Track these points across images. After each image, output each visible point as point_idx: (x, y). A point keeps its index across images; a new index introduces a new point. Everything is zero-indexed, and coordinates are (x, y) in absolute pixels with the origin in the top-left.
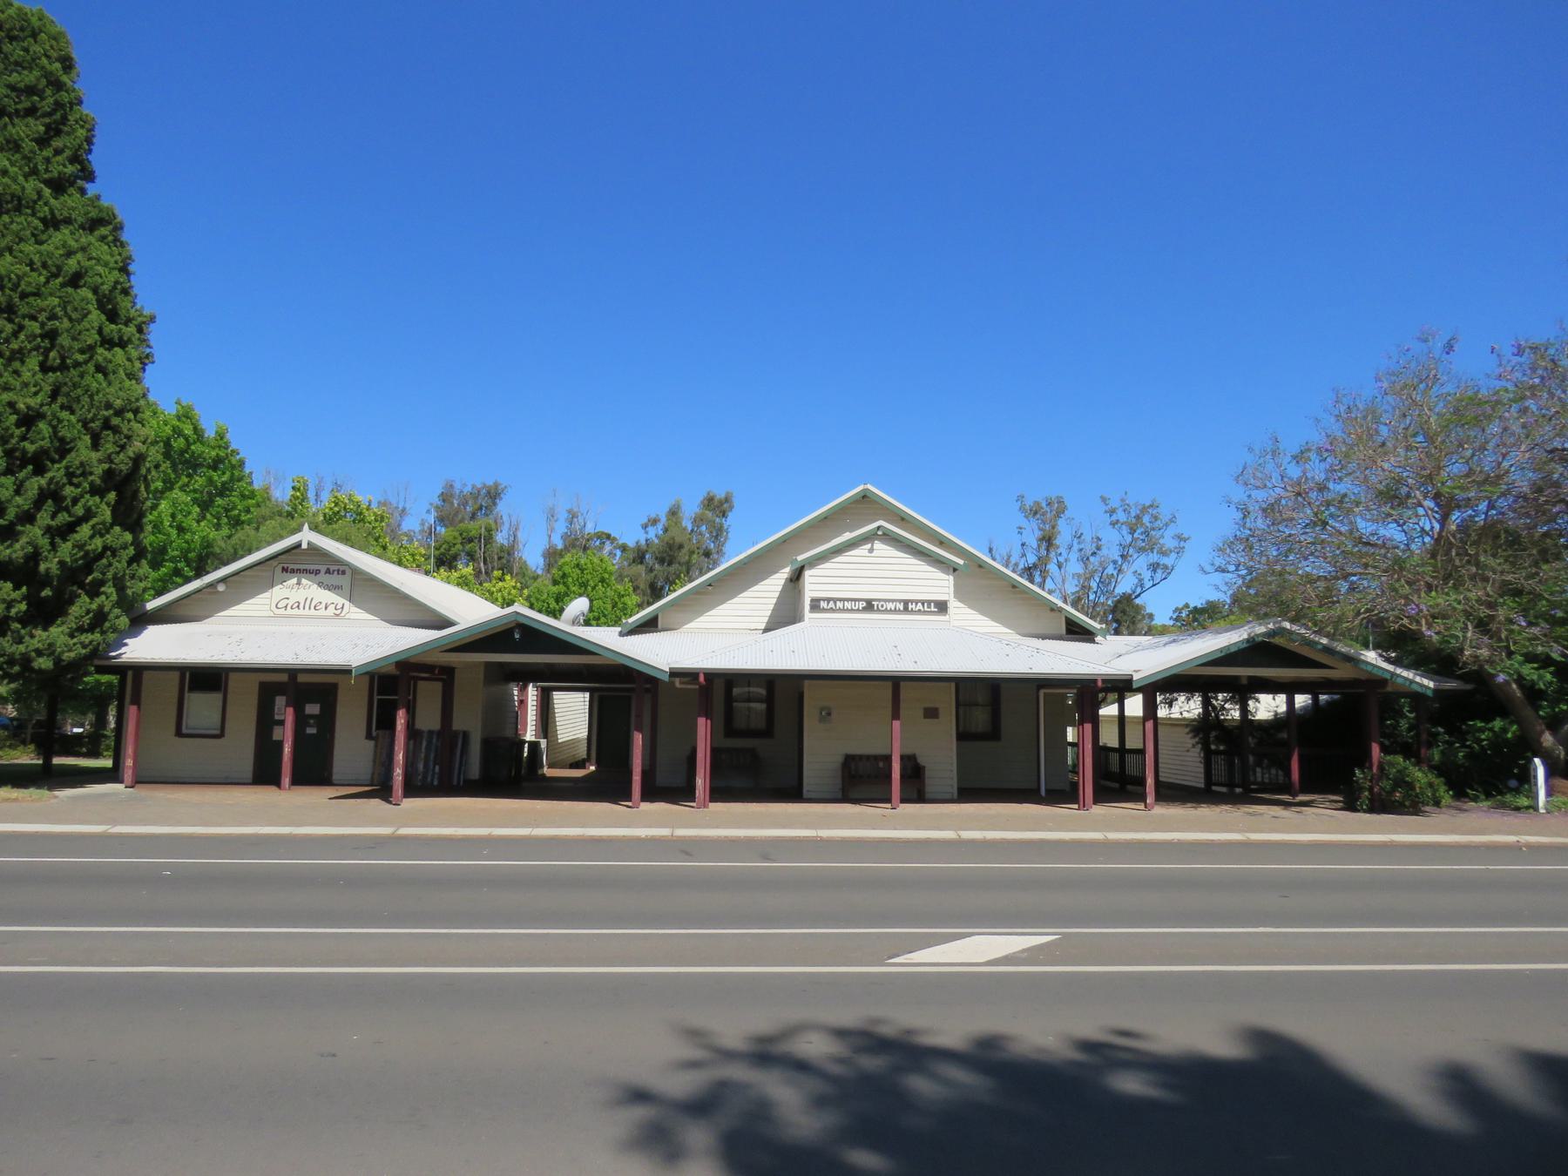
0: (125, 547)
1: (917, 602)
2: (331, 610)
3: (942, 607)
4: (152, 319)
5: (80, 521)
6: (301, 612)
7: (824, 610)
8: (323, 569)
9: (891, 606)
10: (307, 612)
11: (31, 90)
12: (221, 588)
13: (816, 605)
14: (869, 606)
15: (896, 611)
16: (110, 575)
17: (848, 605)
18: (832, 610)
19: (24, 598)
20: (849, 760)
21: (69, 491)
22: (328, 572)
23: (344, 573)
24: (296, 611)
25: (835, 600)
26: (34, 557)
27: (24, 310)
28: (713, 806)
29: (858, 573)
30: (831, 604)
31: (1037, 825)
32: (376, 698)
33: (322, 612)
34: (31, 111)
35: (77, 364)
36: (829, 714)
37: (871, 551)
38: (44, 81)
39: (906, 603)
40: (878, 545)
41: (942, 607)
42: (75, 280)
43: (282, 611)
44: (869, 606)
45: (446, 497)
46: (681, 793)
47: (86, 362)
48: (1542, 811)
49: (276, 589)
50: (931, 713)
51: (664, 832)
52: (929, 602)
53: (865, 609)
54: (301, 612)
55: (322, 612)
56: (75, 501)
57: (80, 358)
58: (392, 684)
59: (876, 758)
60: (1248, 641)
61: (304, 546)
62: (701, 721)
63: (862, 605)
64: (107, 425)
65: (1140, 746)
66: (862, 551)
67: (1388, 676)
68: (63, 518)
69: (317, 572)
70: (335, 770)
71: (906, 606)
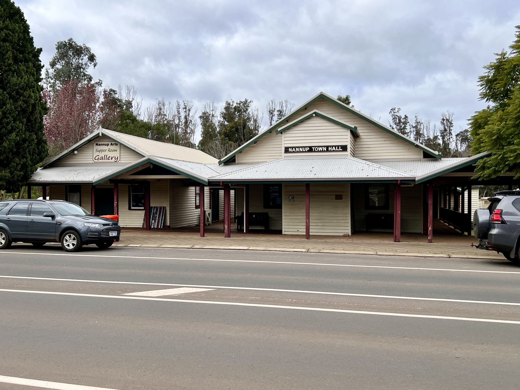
1: (332, 146)
2: (113, 160)
3: (344, 148)
4: (40, 50)
5: (10, 132)
6: (103, 161)
7: (290, 152)
8: (110, 144)
9: (320, 149)
10: (105, 161)
12: (76, 152)
14: (311, 149)
17: (301, 149)
22: (111, 144)
23: (117, 145)
24: (101, 161)
25: (295, 148)
30: (294, 150)
31: (380, 259)
33: (110, 161)
39: (327, 147)
43: (97, 161)
44: (311, 149)
45: (227, 108)
52: (338, 146)
53: (309, 151)
54: (103, 161)
55: (110, 161)
61: (100, 135)
62: (12, 244)
63: (308, 149)
64: (18, 93)
69: (108, 145)
70: (143, 215)
71: (327, 149)
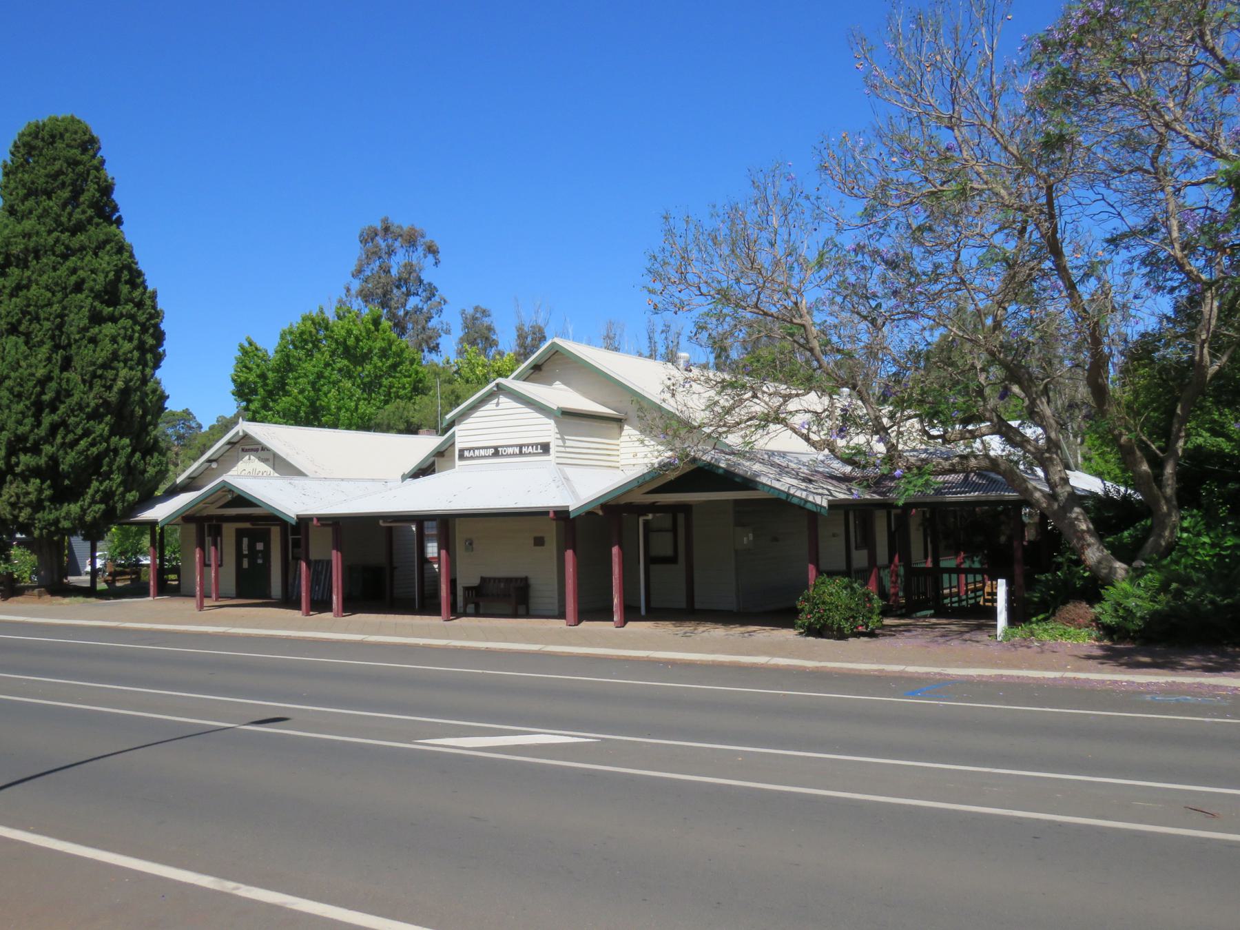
0: (123, 448)
1: (528, 445)
3: (545, 448)
9: (510, 450)
11: (60, 173)
12: (214, 465)
13: (462, 457)
14: (496, 453)
15: (514, 455)
16: (114, 467)
18: (471, 458)
19: (49, 487)
20: (525, 581)
21: (72, 420)
26: (54, 460)
27: (42, 316)
28: (585, 625)
29: (508, 423)
32: (290, 538)
34: (63, 185)
35: (76, 341)
36: (471, 544)
37: (498, 404)
38: (65, 165)
39: (521, 446)
40: (503, 399)
41: (545, 448)
42: (78, 288)
46: (320, 604)
47: (81, 339)
48: (999, 639)
49: (240, 463)
50: (539, 542)
51: (1057, 675)
52: (537, 445)
56: (78, 424)
57: (77, 337)
58: (610, 519)
59: (521, 579)
60: (709, 464)
62: (334, 552)
63: (492, 451)
65: (655, 568)
66: (491, 406)
67: (784, 497)
68: (70, 437)
